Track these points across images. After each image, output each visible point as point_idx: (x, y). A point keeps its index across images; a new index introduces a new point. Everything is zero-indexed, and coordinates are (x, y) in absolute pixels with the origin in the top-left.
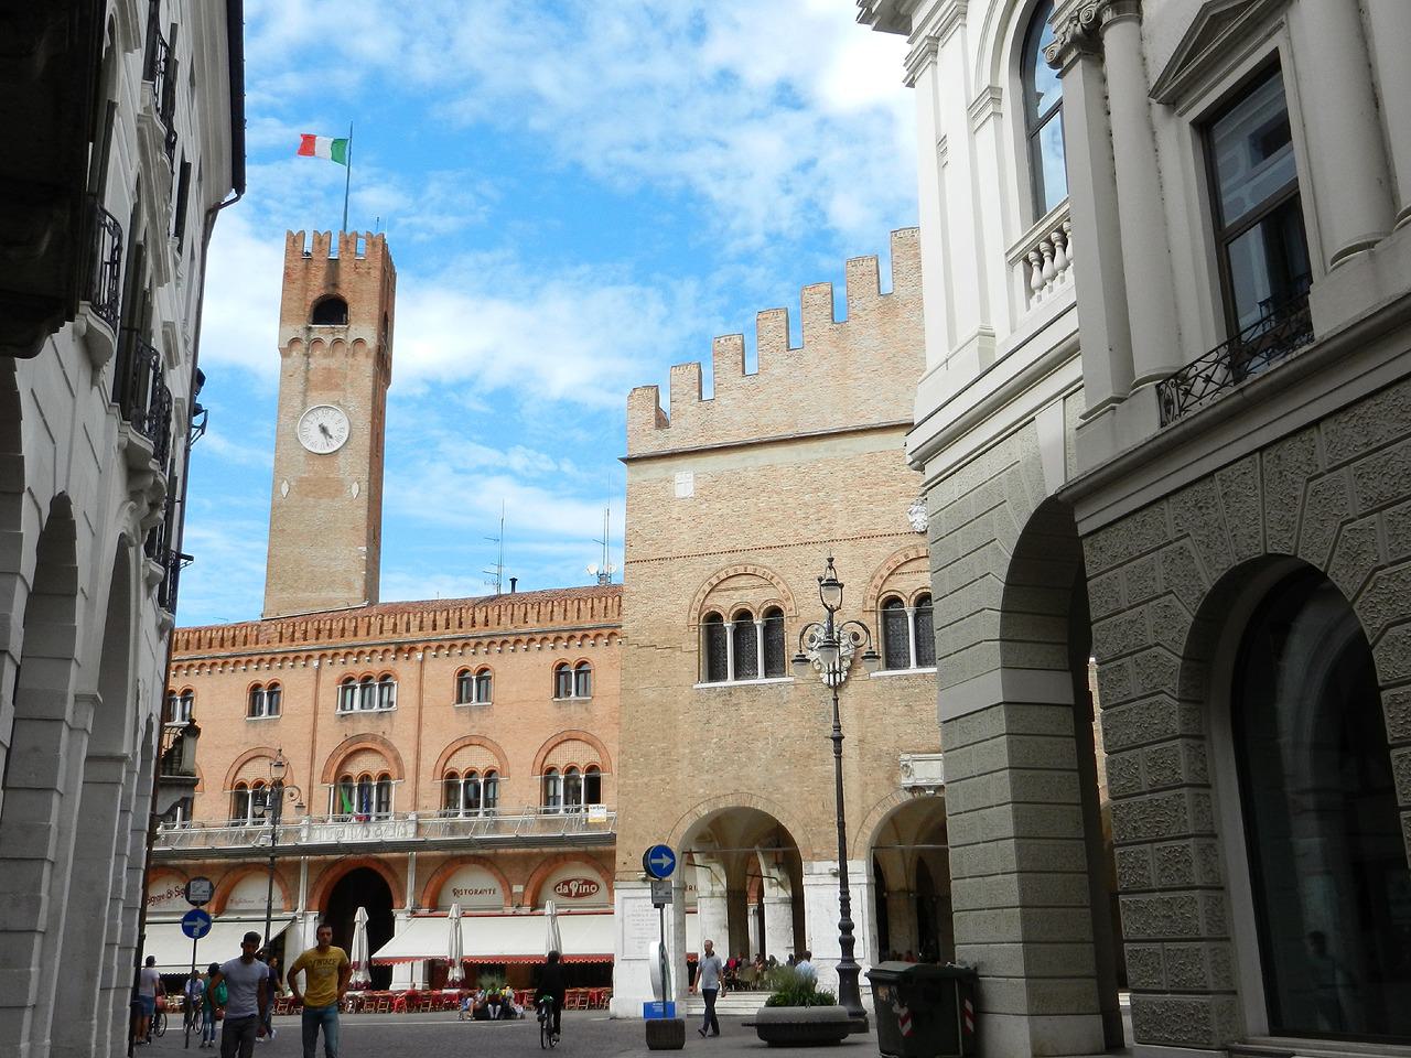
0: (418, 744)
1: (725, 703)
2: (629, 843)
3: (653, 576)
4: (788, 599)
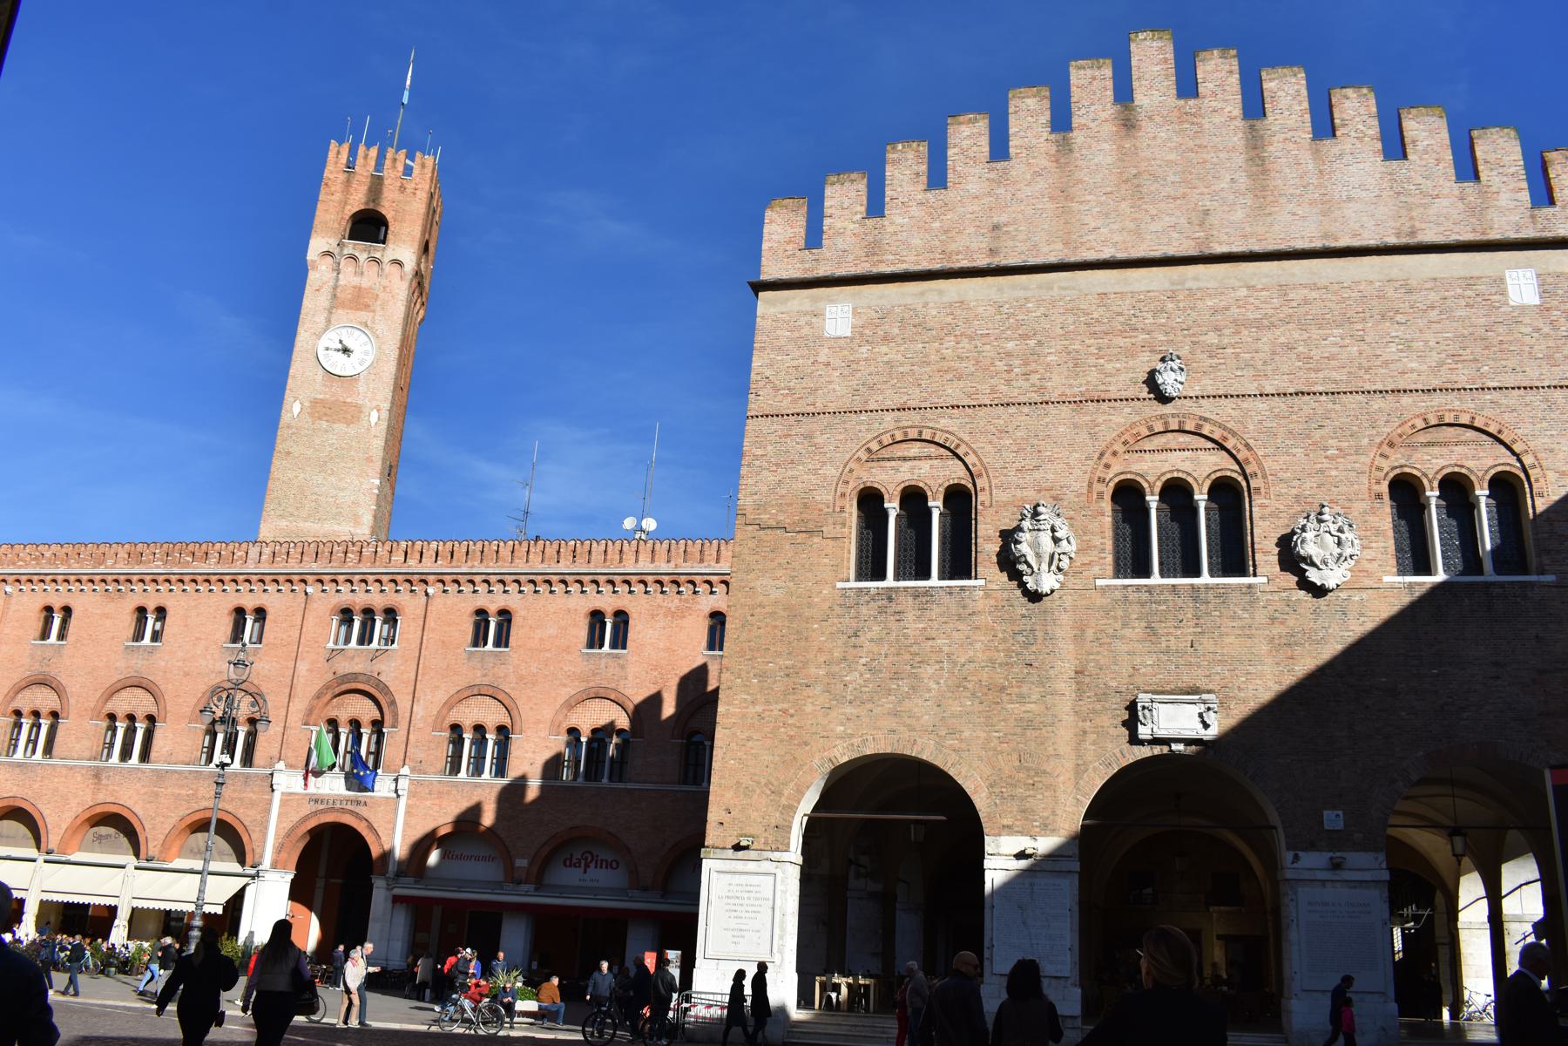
1: (882, 611)
2: (729, 794)
3: (787, 436)
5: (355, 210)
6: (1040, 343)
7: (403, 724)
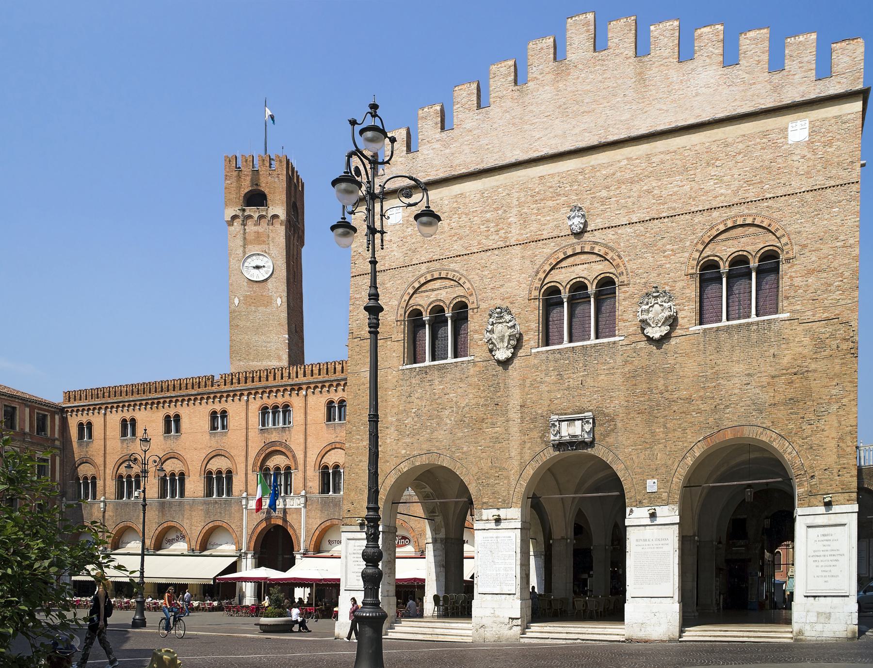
0: (306, 448)
4: (471, 295)
5: (247, 190)
6: (505, 211)
7: (301, 467)
